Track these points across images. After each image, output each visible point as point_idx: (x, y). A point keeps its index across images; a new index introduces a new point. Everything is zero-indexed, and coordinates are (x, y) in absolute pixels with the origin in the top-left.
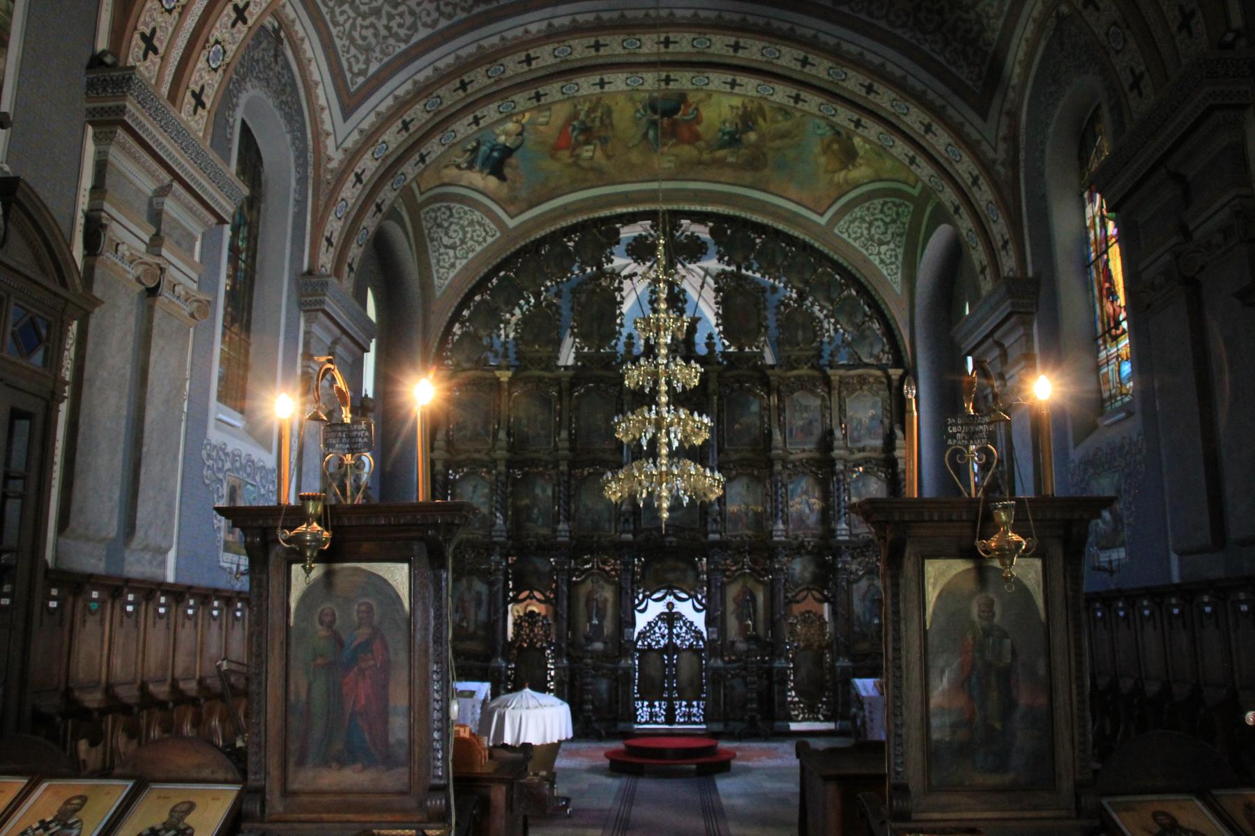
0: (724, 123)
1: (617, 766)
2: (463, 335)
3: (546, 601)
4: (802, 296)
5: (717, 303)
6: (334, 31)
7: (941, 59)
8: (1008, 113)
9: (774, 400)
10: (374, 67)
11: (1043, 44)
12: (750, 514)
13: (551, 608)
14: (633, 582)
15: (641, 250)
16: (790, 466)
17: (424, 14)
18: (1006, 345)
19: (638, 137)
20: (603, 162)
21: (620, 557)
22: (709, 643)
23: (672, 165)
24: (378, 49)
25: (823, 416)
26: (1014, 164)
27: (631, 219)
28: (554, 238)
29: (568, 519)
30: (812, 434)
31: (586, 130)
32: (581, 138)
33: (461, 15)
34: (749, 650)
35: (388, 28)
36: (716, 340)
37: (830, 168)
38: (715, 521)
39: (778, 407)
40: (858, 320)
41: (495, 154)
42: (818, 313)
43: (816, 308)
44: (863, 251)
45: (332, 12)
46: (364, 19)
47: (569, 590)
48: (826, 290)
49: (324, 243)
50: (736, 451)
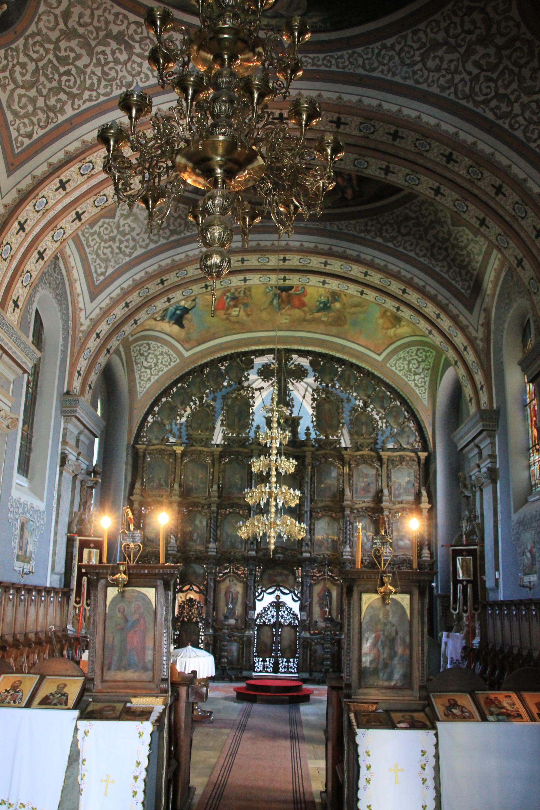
0: (321, 296)
1: (241, 697)
2: (155, 422)
3: (200, 592)
4: (366, 405)
5: (313, 408)
6: (88, 250)
7: (446, 276)
8: (485, 310)
9: (346, 469)
10: (110, 271)
11: (503, 274)
12: (330, 540)
13: (203, 597)
14: (255, 582)
15: (265, 373)
16: (355, 511)
17: (141, 240)
18: (482, 447)
19: (267, 304)
20: (245, 318)
21: (247, 566)
22: (302, 622)
23: (287, 321)
24: (113, 260)
25: (377, 480)
26: (487, 340)
27: (262, 353)
28: (212, 364)
29: (216, 540)
30: (369, 492)
31: (234, 298)
32: (232, 303)
33: (163, 241)
34: (326, 627)
35: (119, 248)
36: (312, 431)
37: (385, 326)
38: (307, 544)
39: (349, 474)
40: (401, 420)
41: (178, 312)
42: (376, 416)
43: (374, 413)
44: (405, 378)
45: (87, 239)
46: (105, 243)
47: (215, 585)
48: (381, 400)
49: (77, 374)
50: (322, 501)
